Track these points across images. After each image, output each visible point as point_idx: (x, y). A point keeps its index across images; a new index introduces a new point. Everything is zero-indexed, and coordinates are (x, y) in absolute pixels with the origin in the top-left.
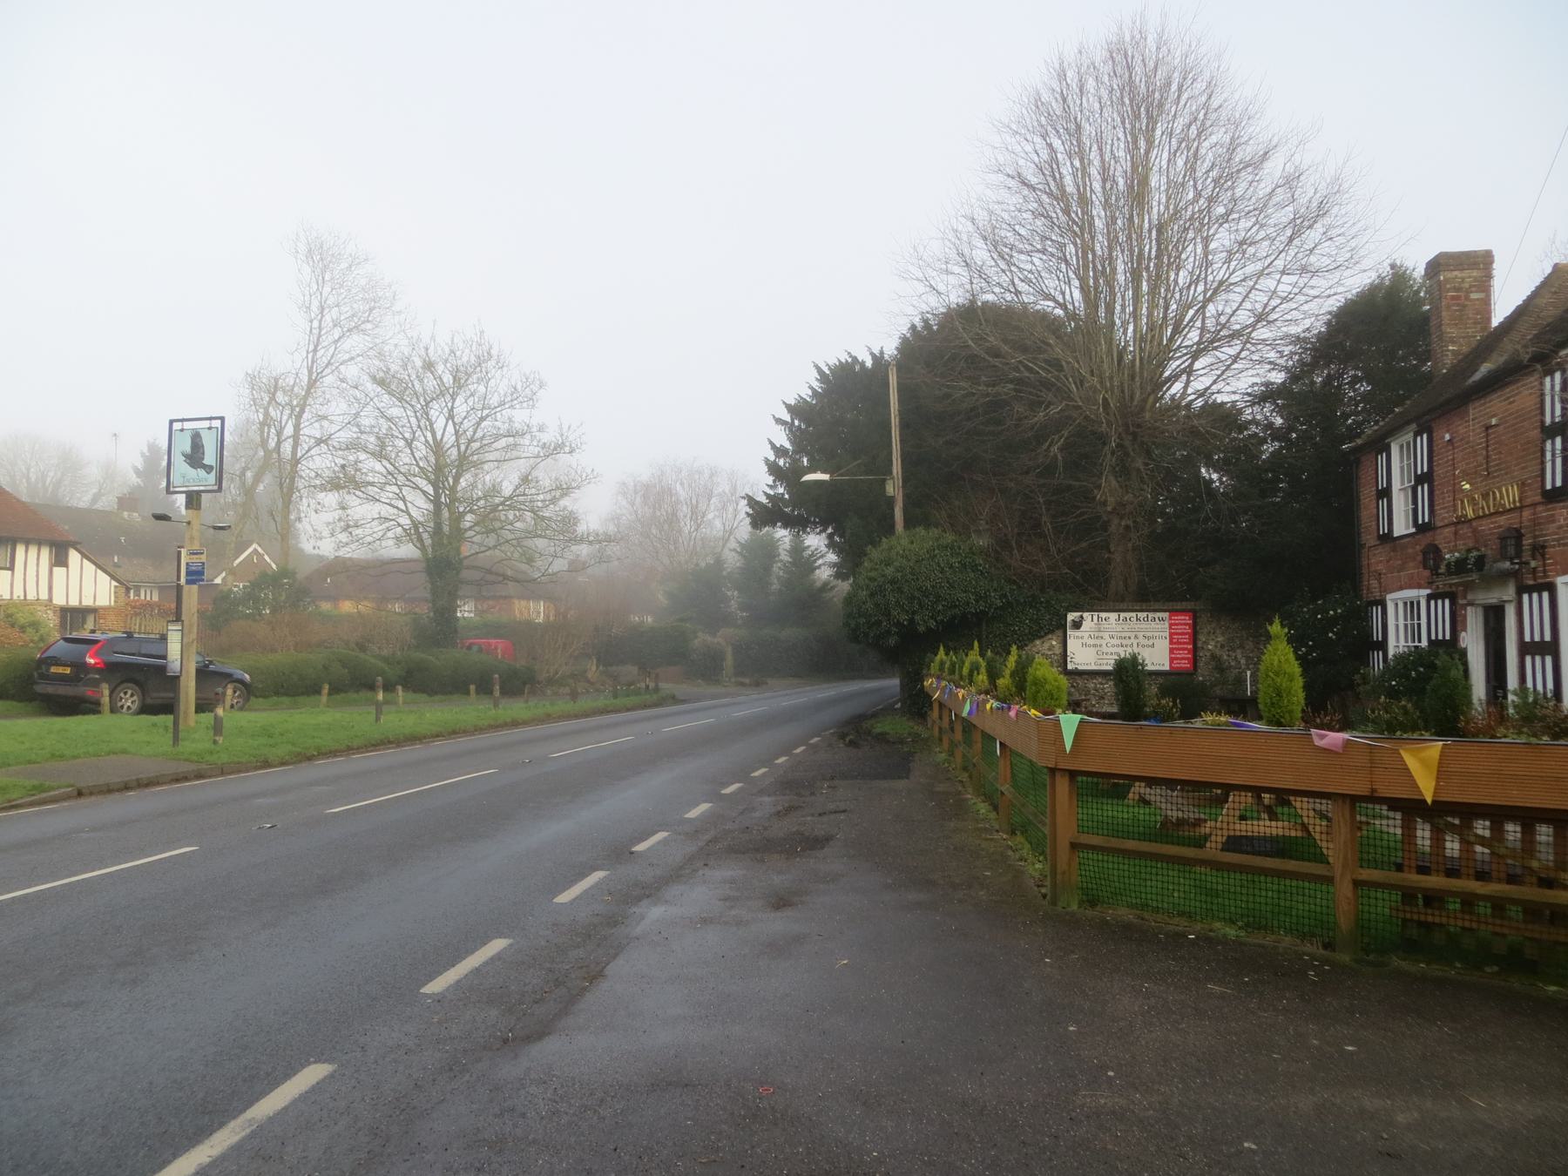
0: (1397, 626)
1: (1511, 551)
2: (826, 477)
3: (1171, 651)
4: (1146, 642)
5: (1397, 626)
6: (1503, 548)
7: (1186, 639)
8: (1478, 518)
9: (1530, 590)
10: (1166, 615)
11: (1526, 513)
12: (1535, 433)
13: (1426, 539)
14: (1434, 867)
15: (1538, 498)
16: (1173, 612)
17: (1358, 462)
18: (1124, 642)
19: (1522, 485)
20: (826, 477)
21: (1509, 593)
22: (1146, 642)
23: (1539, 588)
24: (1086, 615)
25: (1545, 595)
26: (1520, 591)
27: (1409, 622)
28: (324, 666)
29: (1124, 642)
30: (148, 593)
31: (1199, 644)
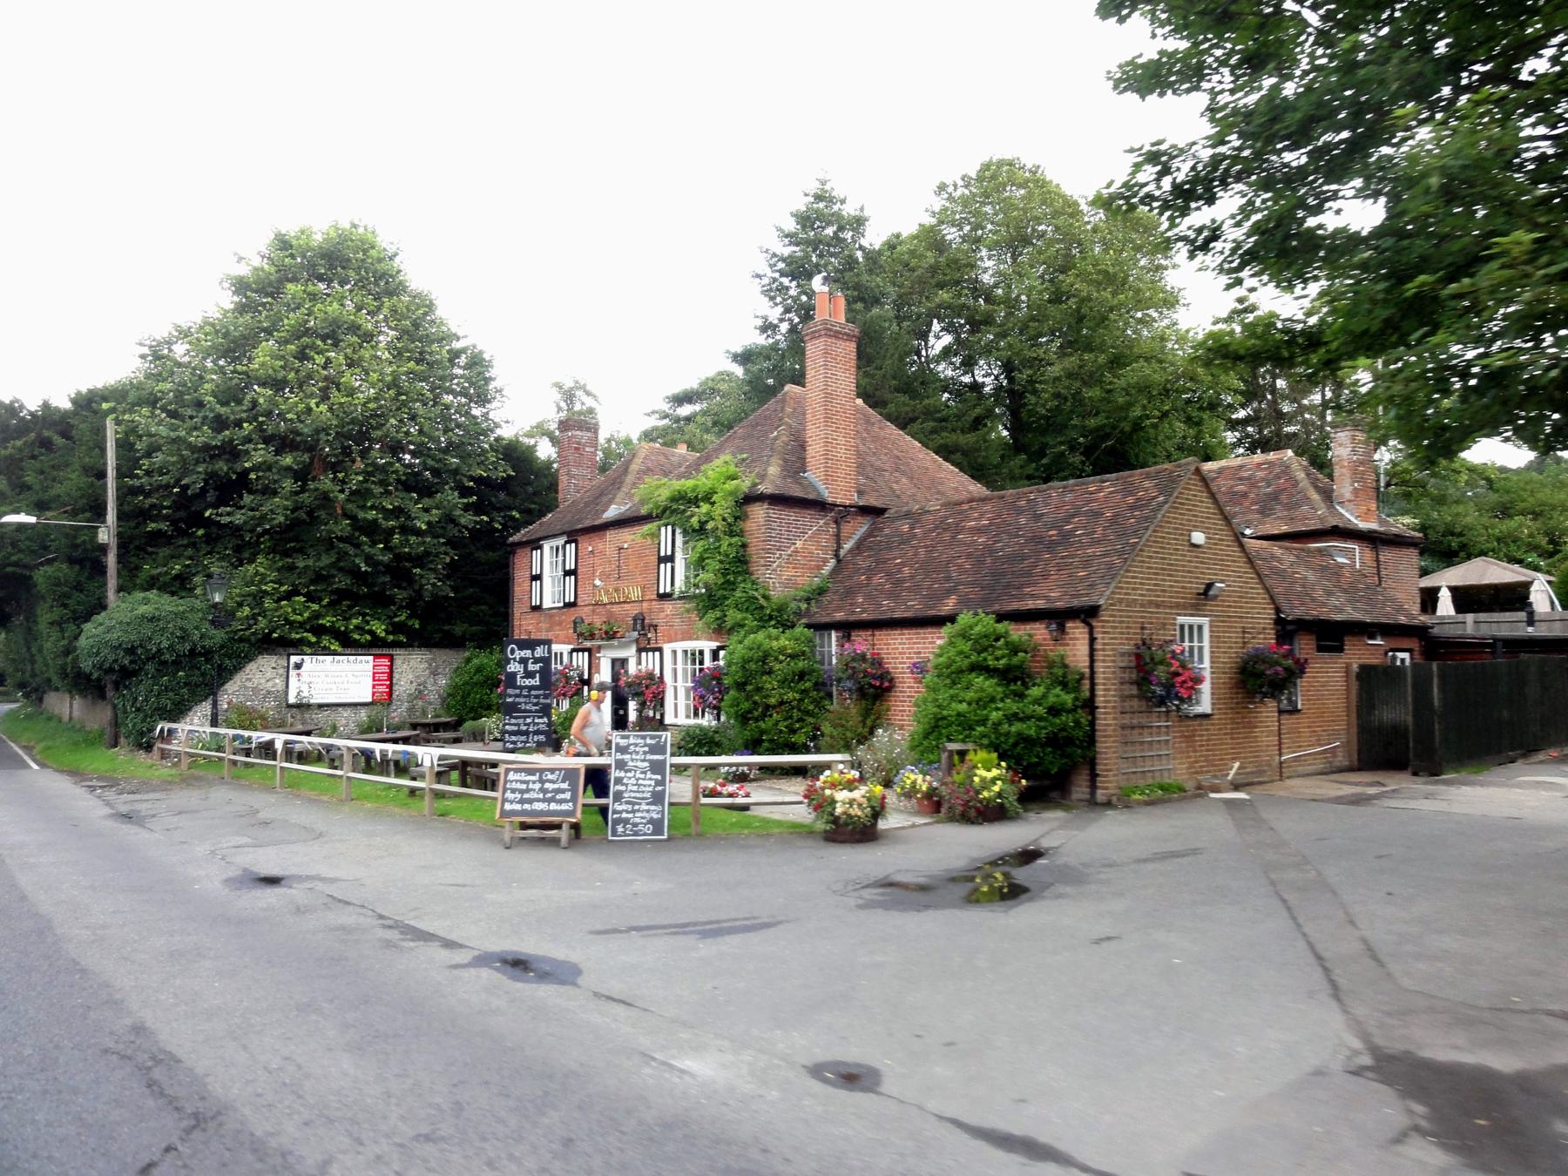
0: (675, 671)
1: (639, 627)
2: (32, 520)
3: (374, 687)
4: (355, 680)
5: (675, 671)
6: (635, 624)
7: (385, 677)
8: (611, 603)
9: (647, 650)
10: (371, 658)
11: (645, 605)
12: (654, 559)
13: (573, 614)
14: (726, 742)
15: (655, 597)
16: (376, 656)
17: (514, 553)
18: (337, 680)
19: (643, 589)
20: (32, 520)
21: (633, 650)
22: (355, 680)
23: (654, 650)
24: (305, 657)
25: (657, 654)
26: (640, 651)
27: (697, 666)
28: (938, 676)
29: (337, 680)
30: (574, 663)
31: (395, 681)
